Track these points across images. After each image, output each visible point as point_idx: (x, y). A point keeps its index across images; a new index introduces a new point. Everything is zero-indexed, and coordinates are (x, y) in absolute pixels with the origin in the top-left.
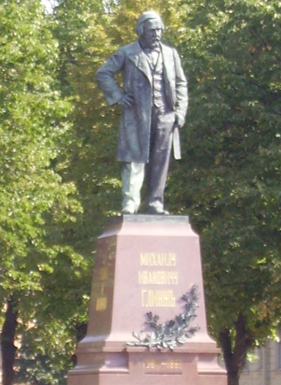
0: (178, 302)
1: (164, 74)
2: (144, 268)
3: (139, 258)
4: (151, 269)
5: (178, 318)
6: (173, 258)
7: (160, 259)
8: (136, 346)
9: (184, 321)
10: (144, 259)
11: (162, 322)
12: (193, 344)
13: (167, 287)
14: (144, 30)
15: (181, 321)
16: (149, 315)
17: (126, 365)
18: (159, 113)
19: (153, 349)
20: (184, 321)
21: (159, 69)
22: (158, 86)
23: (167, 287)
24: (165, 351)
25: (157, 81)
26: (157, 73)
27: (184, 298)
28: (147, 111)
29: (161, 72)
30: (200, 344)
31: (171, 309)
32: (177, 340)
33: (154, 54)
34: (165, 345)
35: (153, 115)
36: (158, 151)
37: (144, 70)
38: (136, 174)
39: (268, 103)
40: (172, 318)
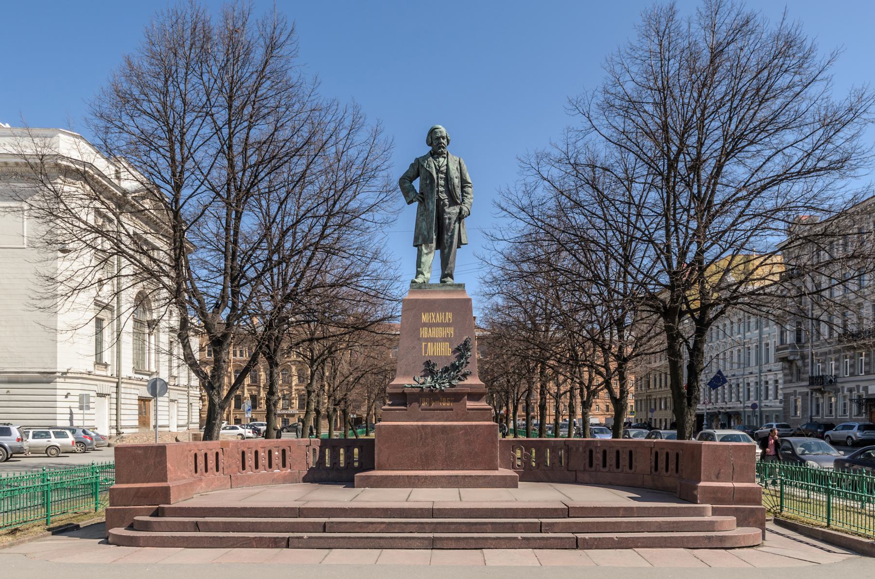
0: (454, 352)
1: (447, 173)
2: (425, 325)
3: (421, 317)
4: (430, 325)
5: (453, 365)
6: (449, 315)
7: (439, 318)
8: (412, 387)
9: (457, 367)
10: (425, 318)
11: (439, 368)
12: (463, 386)
13: (444, 340)
14: (689, 380)
15: (454, 367)
16: (428, 363)
17: (405, 405)
18: (445, 205)
19: (426, 390)
20: (457, 367)
21: (444, 169)
22: (442, 182)
23: (444, 340)
24: (437, 391)
25: (441, 178)
26: (442, 172)
27: (458, 349)
28: (433, 202)
29: (445, 171)
30: (471, 386)
31: (446, 357)
32: (450, 383)
33: (441, 160)
34: (437, 386)
35: (437, 206)
36: (446, 236)
37: (430, 170)
38: (427, 254)
39: (632, 306)
40: (448, 365)
